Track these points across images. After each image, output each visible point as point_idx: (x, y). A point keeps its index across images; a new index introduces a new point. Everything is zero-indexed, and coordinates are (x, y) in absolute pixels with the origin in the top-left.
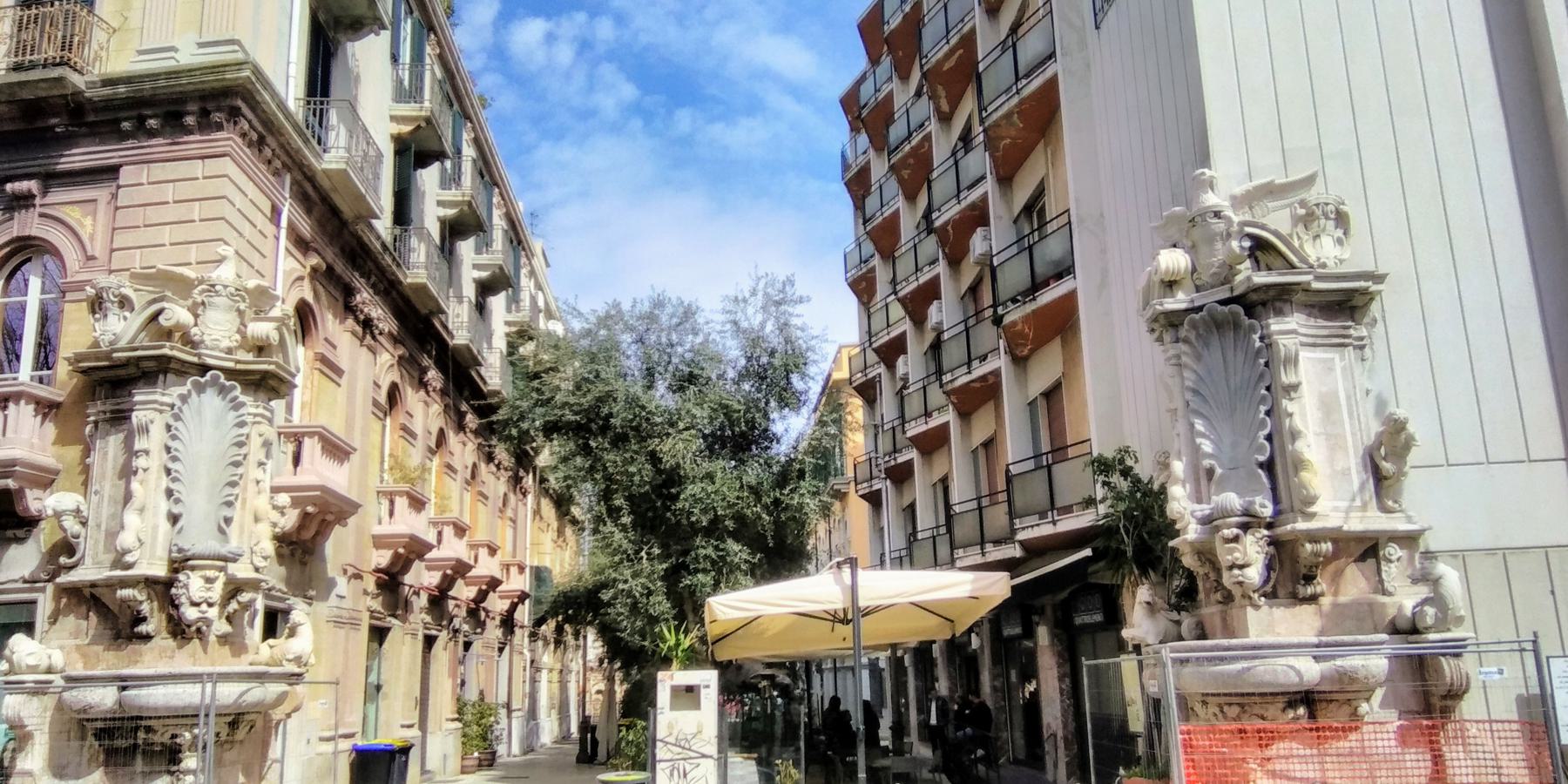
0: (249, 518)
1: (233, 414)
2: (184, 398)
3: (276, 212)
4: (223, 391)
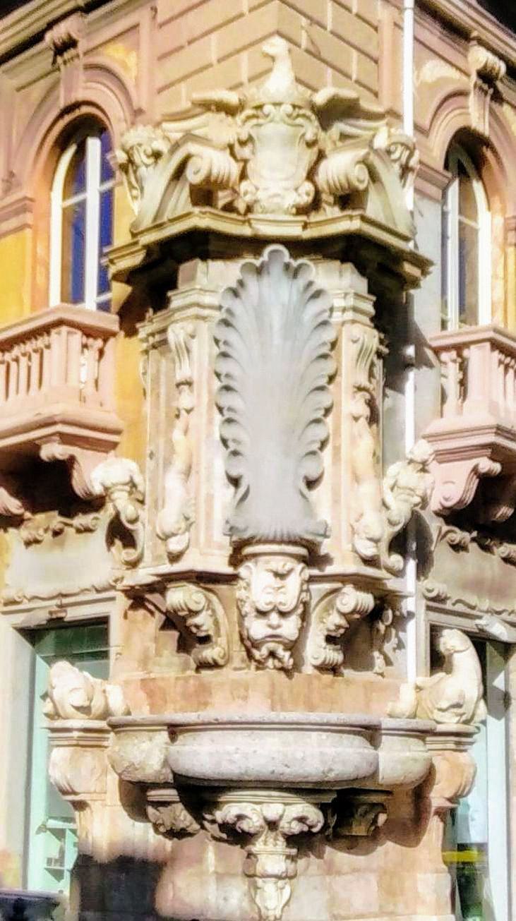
0: (346, 477)
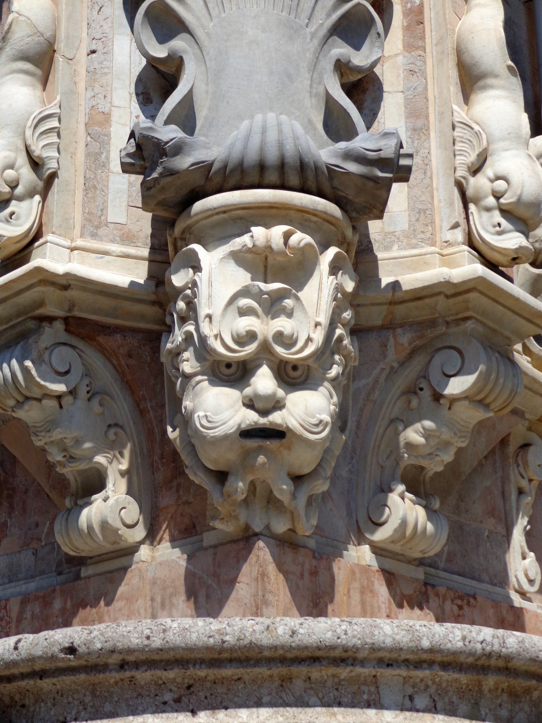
0: (443, 79)
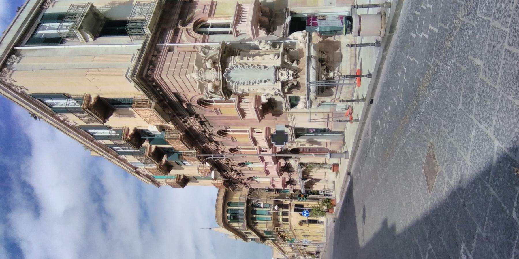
0: (263, 61)
1: (234, 68)
2: (233, 82)
3: (170, 50)
4: (229, 72)
